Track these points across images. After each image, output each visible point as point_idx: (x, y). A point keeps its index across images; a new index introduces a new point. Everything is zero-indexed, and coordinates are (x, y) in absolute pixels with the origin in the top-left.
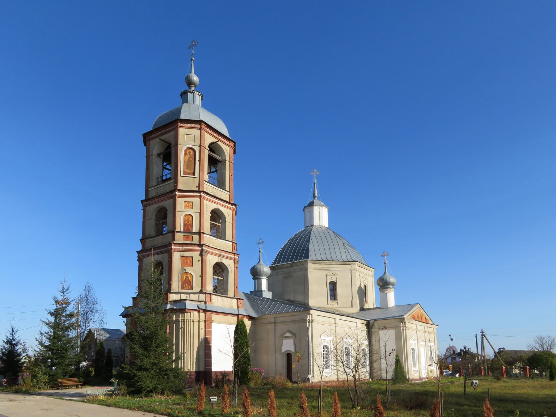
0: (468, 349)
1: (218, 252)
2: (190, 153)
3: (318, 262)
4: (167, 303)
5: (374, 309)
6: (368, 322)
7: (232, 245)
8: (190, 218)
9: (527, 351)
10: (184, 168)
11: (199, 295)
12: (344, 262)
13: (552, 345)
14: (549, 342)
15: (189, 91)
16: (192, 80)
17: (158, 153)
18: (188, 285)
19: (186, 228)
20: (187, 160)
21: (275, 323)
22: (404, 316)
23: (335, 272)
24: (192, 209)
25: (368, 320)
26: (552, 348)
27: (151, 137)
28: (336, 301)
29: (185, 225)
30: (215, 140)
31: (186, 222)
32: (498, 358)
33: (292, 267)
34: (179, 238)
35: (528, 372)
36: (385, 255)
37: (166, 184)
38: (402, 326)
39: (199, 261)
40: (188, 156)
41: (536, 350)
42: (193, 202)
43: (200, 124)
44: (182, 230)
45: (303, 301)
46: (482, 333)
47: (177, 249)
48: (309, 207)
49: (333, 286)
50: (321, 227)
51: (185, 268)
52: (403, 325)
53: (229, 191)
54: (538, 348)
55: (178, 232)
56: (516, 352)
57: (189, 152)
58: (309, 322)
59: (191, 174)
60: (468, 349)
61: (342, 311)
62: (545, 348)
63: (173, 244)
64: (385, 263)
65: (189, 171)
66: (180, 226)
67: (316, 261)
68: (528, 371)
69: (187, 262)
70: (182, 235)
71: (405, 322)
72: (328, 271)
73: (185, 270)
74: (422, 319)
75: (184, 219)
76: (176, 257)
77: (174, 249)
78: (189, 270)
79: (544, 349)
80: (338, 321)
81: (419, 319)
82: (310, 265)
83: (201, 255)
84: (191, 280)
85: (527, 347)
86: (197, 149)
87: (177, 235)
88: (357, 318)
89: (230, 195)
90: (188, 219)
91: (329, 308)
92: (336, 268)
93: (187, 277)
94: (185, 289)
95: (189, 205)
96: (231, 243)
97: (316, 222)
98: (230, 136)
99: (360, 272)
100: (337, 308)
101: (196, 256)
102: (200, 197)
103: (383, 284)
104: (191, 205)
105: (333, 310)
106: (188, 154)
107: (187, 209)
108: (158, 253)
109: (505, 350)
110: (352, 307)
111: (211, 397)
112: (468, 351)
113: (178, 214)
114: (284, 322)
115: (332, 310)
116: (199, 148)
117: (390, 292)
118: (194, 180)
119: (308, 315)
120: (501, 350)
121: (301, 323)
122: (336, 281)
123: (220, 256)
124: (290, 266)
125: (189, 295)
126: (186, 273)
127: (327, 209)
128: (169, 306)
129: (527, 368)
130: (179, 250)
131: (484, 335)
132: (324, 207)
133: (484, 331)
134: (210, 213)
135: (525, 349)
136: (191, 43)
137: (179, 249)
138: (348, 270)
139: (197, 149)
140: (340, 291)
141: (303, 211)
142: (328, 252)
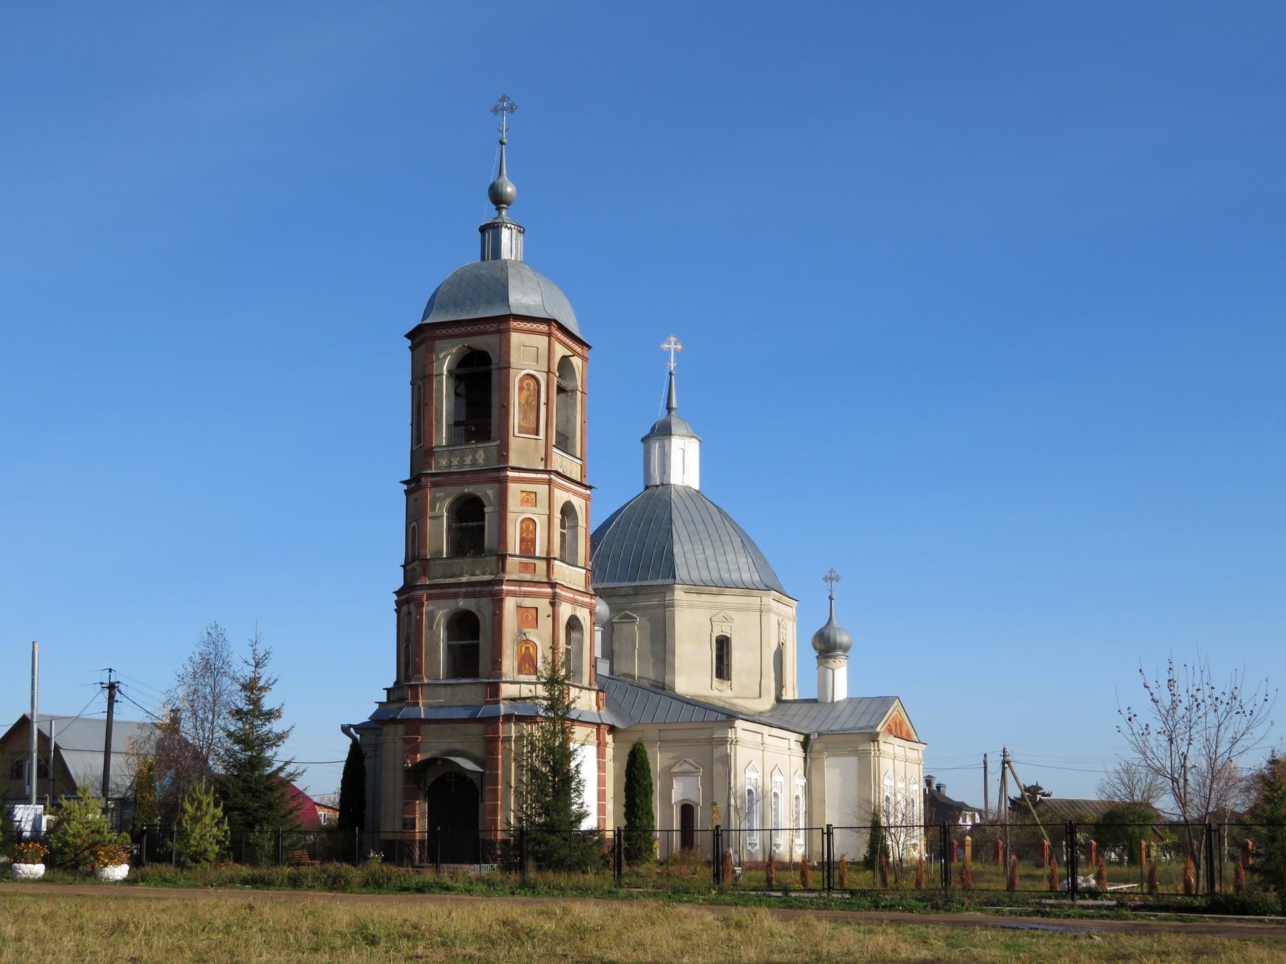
0: (939, 787)
1: (571, 595)
2: (529, 385)
3: (697, 587)
4: (497, 702)
5: (795, 701)
6: (807, 737)
7: (586, 575)
8: (531, 527)
9: (1098, 802)
10: (519, 418)
11: (536, 687)
12: (749, 588)
13: (1152, 789)
14: (1146, 781)
15: (505, 225)
16: (502, 193)
17: (451, 368)
18: (529, 666)
19: (523, 547)
22: (876, 726)
23: (731, 614)
24: (534, 508)
25: (806, 732)
26: (1151, 797)
27: (437, 332)
28: (729, 682)
29: (522, 540)
30: (570, 353)
31: (525, 535)
32: (1035, 819)
33: (637, 594)
34: (513, 568)
35: (1094, 858)
36: (831, 579)
37: (481, 446)
38: (873, 749)
39: (548, 616)
40: (525, 393)
41: (1117, 800)
42: (535, 493)
43: (549, 325)
44: (518, 552)
45: (661, 681)
46: (1004, 756)
47: (511, 591)
48: (658, 438)
49: (723, 645)
50: (687, 489)
51: (525, 630)
52: (874, 746)
53: (580, 457)
54: (1121, 796)
55: (511, 555)
56: (1072, 803)
57: (527, 385)
58: (731, 744)
59: (531, 432)
60: (939, 787)
61: (740, 706)
62: (1138, 797)
63: (505, 582)
64: (831, 598)
65: (528, 425)
66: (514, 545)
67: (692, 586)
68: (1093, 851)
69: (527, 616)
71: (878, 741)
72: (715, 612)
73: (525, 634)
74: (901, 733)
75: (521, 528)
76: (510, 604)
77: (507, 591)
78: (532, 635)
79: (1135, 798)
80: (767, 740)
81: (899, 732)
82: (679, 594)
83: (553, 604)
84: (533, 655)
85: (1099, 793)
86: (542, 378)
87: (509, 560)
88: (791, 731)
89: (581, 466)
91: (714, 699)
92: (732, 605)
93: (527, 648)
94: (524, 672)
95: (528, 499)
96: (584, 571)
97: (676, 478)
98: (581, 332)
99: (779, 615)
100: (729, 698)
101: (544, 605)
102: (550, 482)
103: (826, 647)
104: (532, 499)
105: (723, 703)
106: (525, 387)
108: (467, 596)
109: (1048, 798)
110: (760, 696)
111: (736, 868)
112: (936, 794)
113: (510, 517)
114: (680, 741)
115: (720, 703)
116: (545, 375)
117: (839, 668)
118: (537, 444)
119: (730, 730)
120: (1038, 799)
122: (729, 636)
123: (574, 602)
124: (631, 592)
125: (534, 686)
126: (527, 641)
127: (698, 442)
128: (503, 708)
129: (1092, 844)
130: (514, 594)
131: (1008, 762)
132: (693, 439)
133: (1009, 751)
135: (1093, 797)
136: (500, 101)
137: (515, 591)
138: (754, 610)
139: (542, 378)
140: (738, 658)
141: (643, 440)
142: (712, 564)
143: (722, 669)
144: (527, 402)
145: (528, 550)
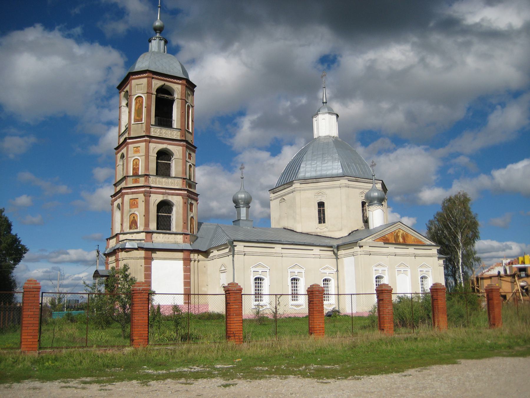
2: (139, 101)
20: (137, 109)
21: (338, 295)
23: (324, 190)
29: (134, 169)
31: (135, 166)
40: (138, 104)
44: (131, 174)
70: (131, 178)
90: (136, 163)
93: (134, 217)
101: (141, 197)
107: (135, 155)
118: (142, 125)
121: (163, 233)
123: (163, 194)
130: (127, 193)
134: (157, 154)
137: (128, 192)
143: (322, 219)
144: (138, 108)
145: (136, 173)
